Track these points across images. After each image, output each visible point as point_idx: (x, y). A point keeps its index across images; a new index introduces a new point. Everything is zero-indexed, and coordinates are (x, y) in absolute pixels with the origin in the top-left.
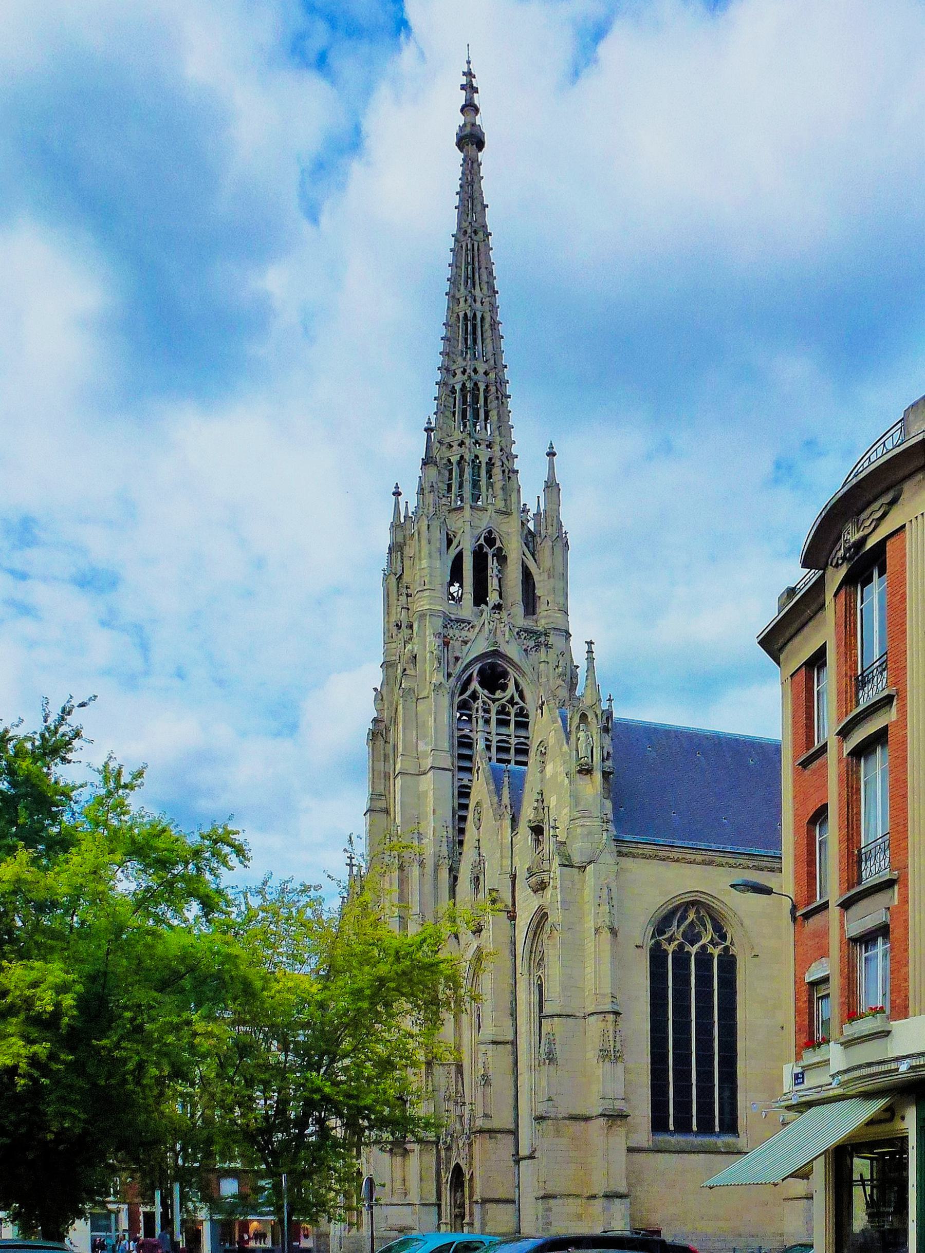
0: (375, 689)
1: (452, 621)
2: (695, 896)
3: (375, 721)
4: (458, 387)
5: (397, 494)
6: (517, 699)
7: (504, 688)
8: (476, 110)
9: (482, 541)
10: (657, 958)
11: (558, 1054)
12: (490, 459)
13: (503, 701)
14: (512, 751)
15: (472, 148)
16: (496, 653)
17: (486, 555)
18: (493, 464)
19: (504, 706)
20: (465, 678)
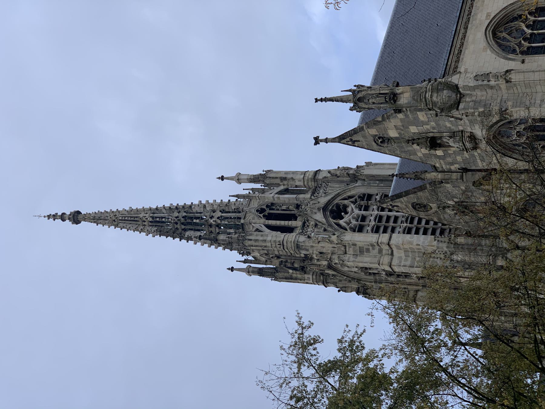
0: (339, 291)
1: (303, 232)
2: (489, 34)
3: (358, 293)
4: (183, 227)
5: (232, 269)
8: (63, 214)
9: (261, 215)
10: (531, 51)
12: (220, 211)
15: (80, 217)
16: (324, 209)
17: (269, 214)
18: (224, 210)
20: (337, 227)
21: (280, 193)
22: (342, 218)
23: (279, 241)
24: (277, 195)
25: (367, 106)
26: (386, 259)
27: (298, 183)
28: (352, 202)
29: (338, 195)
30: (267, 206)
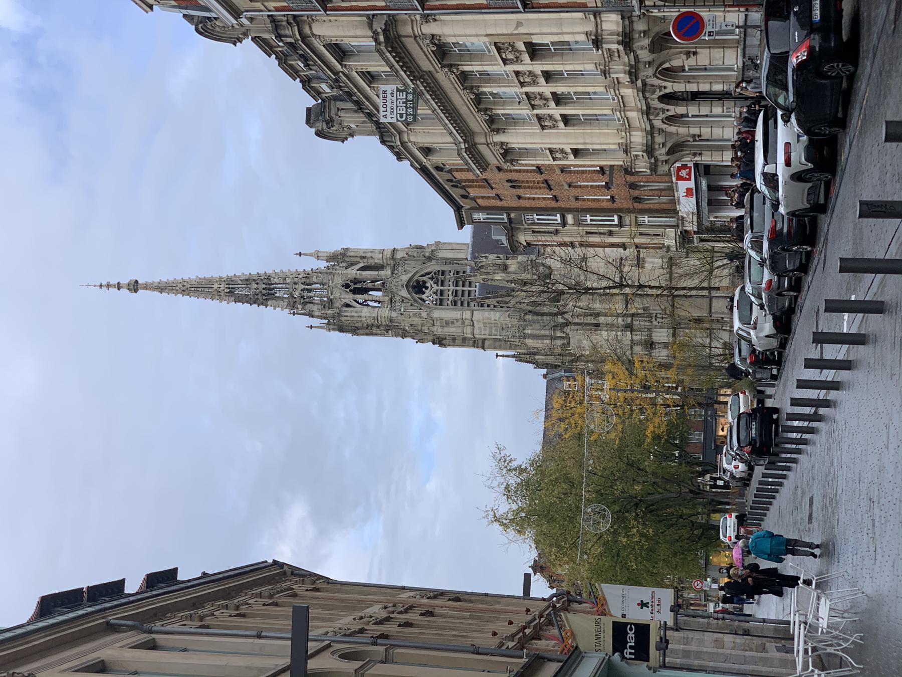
3: (434, 343)
4: (264, 297)
5: (311, 327)
6: (430, 276)
7: (425, 282)
9: (348, 290)
11: (758, 326)
12: (302, 284)
14: (457, 288)
19: (435, 283)
21: (362, 269)
22: (424, 293)
23: (374, 317)
24: (359, 272)
25: (486, 271)
26: (468, 330)
27: (377, 261)
28: (430, 278)
29: (417, 272)
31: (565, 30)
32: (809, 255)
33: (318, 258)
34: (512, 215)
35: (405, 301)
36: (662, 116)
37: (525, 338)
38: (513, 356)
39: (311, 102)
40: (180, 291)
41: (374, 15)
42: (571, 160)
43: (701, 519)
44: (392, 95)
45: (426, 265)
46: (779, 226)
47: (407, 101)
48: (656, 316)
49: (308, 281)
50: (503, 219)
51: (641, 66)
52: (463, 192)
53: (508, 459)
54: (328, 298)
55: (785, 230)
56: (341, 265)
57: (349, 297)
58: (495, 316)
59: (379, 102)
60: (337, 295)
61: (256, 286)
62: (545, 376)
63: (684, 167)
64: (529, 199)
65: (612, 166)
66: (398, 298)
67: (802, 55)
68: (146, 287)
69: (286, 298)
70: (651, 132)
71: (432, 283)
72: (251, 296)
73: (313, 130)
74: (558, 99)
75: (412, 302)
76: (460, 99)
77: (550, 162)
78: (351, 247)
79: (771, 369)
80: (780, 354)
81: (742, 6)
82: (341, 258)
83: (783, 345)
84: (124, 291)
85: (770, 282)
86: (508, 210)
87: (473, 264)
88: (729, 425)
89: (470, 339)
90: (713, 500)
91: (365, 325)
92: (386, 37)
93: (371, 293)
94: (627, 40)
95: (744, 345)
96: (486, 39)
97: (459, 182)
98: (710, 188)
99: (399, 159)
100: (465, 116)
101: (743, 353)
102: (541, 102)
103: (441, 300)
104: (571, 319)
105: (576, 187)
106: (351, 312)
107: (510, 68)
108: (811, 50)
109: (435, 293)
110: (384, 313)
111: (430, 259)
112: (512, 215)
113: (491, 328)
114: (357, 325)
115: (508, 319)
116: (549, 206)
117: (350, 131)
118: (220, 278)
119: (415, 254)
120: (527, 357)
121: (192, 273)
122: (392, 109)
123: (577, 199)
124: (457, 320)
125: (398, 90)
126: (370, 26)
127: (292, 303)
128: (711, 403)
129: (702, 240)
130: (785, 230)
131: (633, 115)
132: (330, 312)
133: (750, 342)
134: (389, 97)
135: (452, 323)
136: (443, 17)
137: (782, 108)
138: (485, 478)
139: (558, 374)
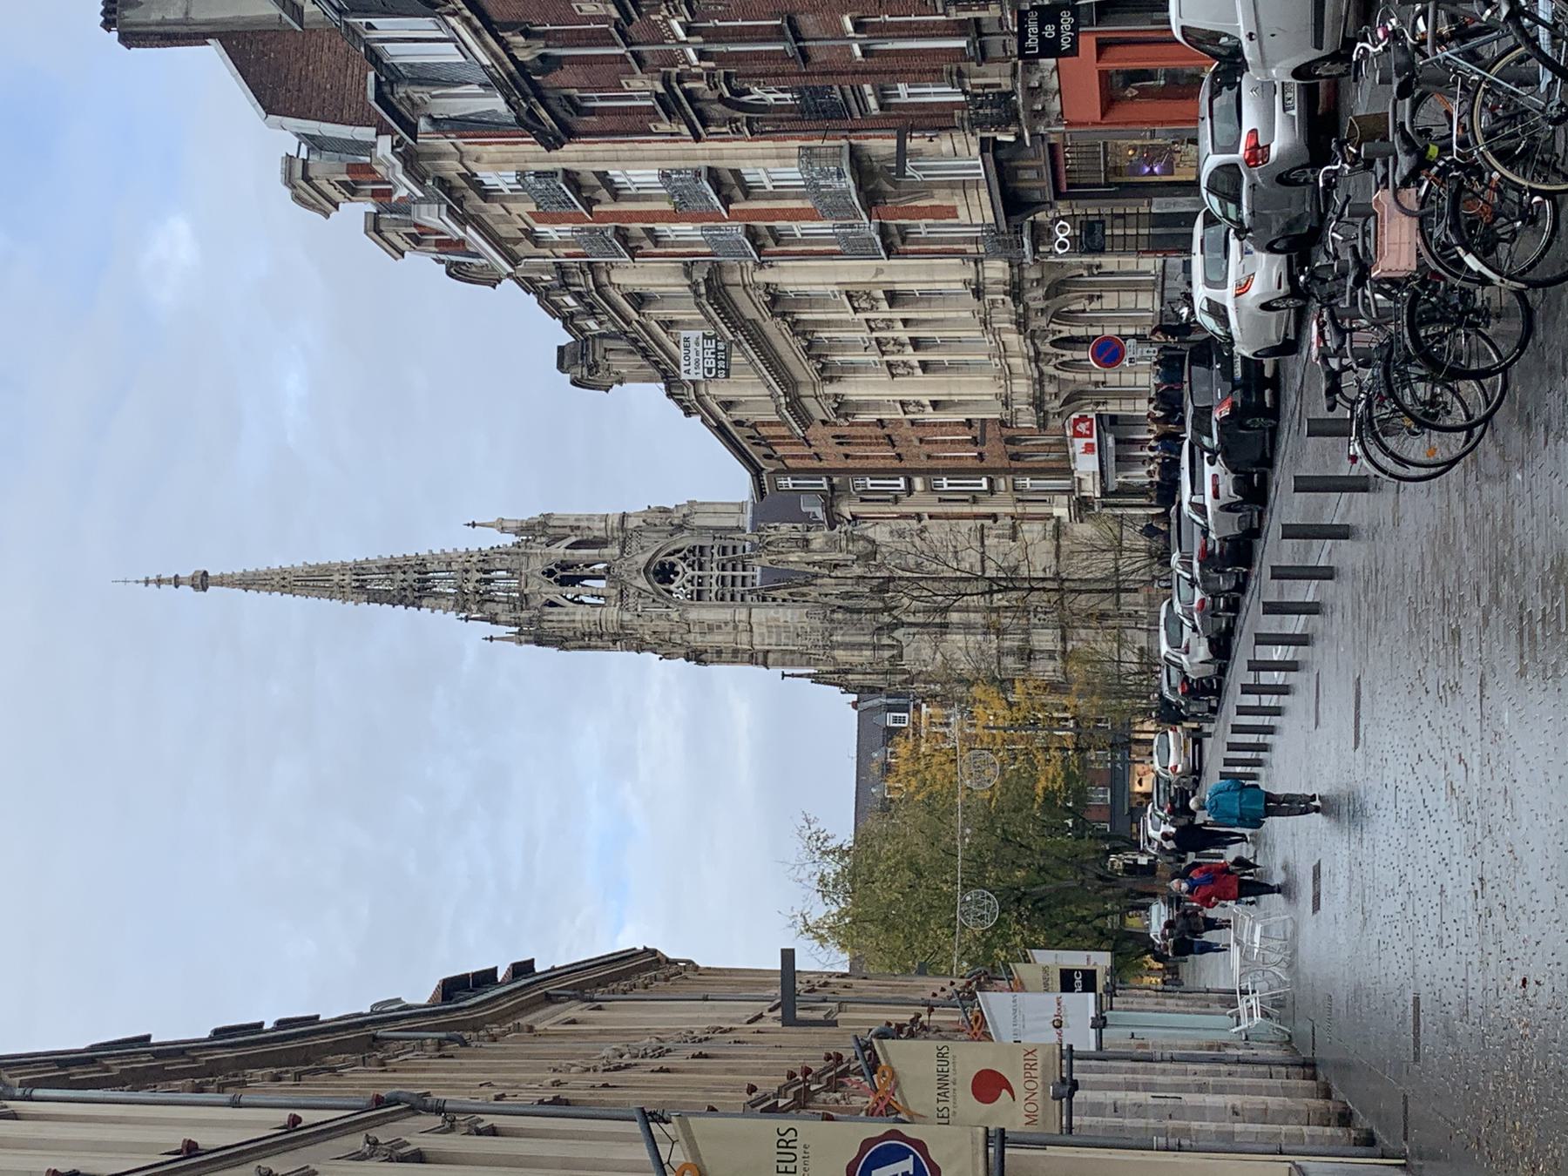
3: (688, 660)
4: (417, 594)
6: (681, 555)
7: (673, 565)
9: (552, 580)
13: (685, 565)
14: (725, 573)
19: (689, 566)
22: (672, 582)
24: (568, 551)
26: (745, 637)
27: (597, 533)
30: (557, 566)
31: (937, 278)
32: (1246, 576)
33: (503, 530)
34: (835, 480)
35: (644, 594)
36: (1054, 361)
37: (832, 648)
38: (809, 676)
39: (566, 339)
40: (277, 586)
41: (692, 262)
42: (930, 415)
43: (1111, 923)
44: (697, 344)
45: (675, 538)
46: (1210, 546)
47: (717, 351)
48: (1035, 610)
49: (486, 567)
50: (822, 485)
51: (1032, 314)
52: (767, 451)
53: (822, 836)
54: (521, 593)
55: (1217, 551)
56: (538, 540)
57: (553, 591)
58: (790, 615)
59: (680, 353)
60: (535, 588)
61: (403, 576)
62: (855, 705)
63: (1083, 419)
64: (861, 457)
65: (983, 420)
66: (632, 591)
67: (1226, 411)
68: (222, 581)
69: (451, 594)
70: (1040, 380)
71: (685, 565)
72: (395, 593)
73: (567, 377)
74: (916, 344)
75: (655, 597)
76: (787, 347)
77: (901, 416)
78: (558, 511)
79: (1209, 701)
80: (1220, 683)
81: (1157, 252)
82: (538, 530)
83: (1222, 671)
84: (186, 589)
85: (1202, 601)
86: (829, 473)
87: (756, 540)
88: (1153, 775)
89: (745, 651)
90: (1131, 890)
91: (578, 634)
92: (709, 289)
93: (586, 582)
94: (1016, 290)
95: (1174, 671)
96: (836, 288)
97: (763, 438)
98: (1117, 442)
99: (688, 413)
100: (790, 366)
101: (1173, 682)
102: (895, 349)
103: (699, 592)
104: (904, 618)
105: (929, 442)
106: (559, 614)
107: (862, 316)
108: (1233, 406)
109: (690, 581)
110: (612, 614)
111: (680, 528)
112: (835, 480)
113: (779, 635)
114: (565, 634)
115: (805, 619)
116: (888, 466)
117: (617, 378)
118: (344, 565)
119: (657, 522)
120: (836, 677)
121: (278, 562)
122: (697, 362)
123: (929, 457)
124: (726, 623)
125: (705, 336)
126: (688, 274)
127: (461, 602)
128: (1125, 744)
129: (1105, 506)
130: (1217, 551)
131: (1017, 362)
132: (524, 615)
133: (1181, 667)
134: (693, 346)
135: (719, 627)
136: (780, 264)
137: (1208, 450)
138: (789, 867)
139: (876, 702)
